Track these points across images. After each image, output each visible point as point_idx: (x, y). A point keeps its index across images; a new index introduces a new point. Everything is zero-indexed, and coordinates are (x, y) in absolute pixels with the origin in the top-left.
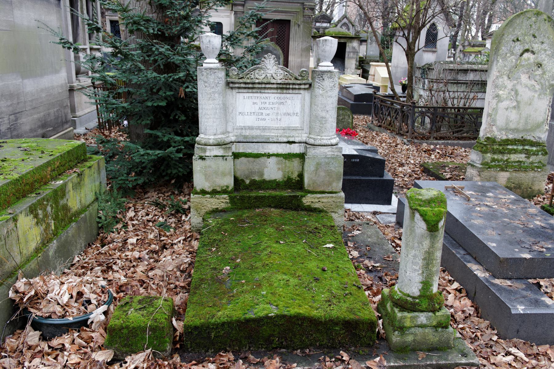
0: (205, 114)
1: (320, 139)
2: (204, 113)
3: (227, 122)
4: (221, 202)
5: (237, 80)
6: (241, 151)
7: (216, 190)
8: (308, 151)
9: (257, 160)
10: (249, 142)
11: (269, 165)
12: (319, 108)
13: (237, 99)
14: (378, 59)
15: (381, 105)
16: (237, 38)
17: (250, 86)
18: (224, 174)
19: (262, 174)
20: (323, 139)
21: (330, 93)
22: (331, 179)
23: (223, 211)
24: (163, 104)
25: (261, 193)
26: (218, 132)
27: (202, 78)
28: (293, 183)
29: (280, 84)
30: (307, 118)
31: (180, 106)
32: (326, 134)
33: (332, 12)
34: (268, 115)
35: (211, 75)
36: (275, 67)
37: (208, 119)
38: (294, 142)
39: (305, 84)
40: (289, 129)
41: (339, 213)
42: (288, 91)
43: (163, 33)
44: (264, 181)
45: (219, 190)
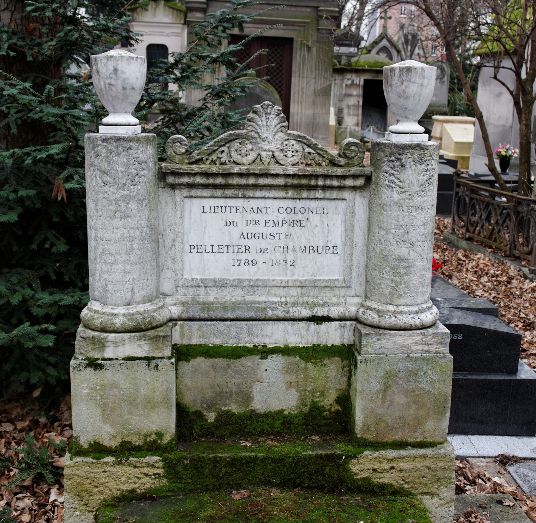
0: (103, 253)
1: (394, 312)
2: (100, 250)
3: (159, 269)
4: (142, 475)
5: (184, 167)
6: (195, 341)
7: (129, 443)
8: (364, 342)
9: (236, 363)
10: (216, 320)
11: (265, 374)
12: (390, 236)
13: (187, 213)
14: (446, 109)
15: (471, 199)
16: (189, 67)
17: (219, 181)
18: (151, 404)
19: (247, 399)
20: (401, 312)
21: (418, 200)
22: (422, 412)
23: (148, 497)
24: (12, 217)
25: (246, 448)
26: (138, 296)
27: (96, 162)
28: (325, 418)
29: (293, 176)
30: (359, 259)
31: (55, 219)
32: (408, 300)
33: (358, 28)
34: (263, 251)
35: (118, 155)
36: (280, 134)
37: (111, 264)
38: (327, 319)
39: (355, 177)
40: (315, 285)
41: (442, 496)
42: (312, 194)
43: (23, 55)
44: (253, 415)
45: (137, 442)
